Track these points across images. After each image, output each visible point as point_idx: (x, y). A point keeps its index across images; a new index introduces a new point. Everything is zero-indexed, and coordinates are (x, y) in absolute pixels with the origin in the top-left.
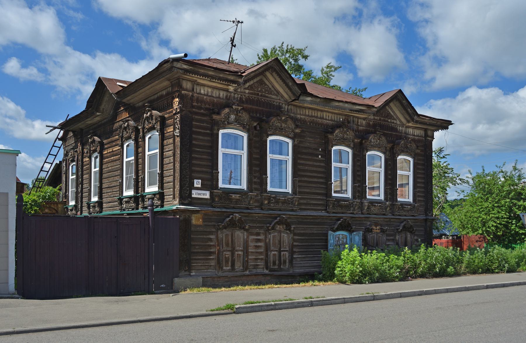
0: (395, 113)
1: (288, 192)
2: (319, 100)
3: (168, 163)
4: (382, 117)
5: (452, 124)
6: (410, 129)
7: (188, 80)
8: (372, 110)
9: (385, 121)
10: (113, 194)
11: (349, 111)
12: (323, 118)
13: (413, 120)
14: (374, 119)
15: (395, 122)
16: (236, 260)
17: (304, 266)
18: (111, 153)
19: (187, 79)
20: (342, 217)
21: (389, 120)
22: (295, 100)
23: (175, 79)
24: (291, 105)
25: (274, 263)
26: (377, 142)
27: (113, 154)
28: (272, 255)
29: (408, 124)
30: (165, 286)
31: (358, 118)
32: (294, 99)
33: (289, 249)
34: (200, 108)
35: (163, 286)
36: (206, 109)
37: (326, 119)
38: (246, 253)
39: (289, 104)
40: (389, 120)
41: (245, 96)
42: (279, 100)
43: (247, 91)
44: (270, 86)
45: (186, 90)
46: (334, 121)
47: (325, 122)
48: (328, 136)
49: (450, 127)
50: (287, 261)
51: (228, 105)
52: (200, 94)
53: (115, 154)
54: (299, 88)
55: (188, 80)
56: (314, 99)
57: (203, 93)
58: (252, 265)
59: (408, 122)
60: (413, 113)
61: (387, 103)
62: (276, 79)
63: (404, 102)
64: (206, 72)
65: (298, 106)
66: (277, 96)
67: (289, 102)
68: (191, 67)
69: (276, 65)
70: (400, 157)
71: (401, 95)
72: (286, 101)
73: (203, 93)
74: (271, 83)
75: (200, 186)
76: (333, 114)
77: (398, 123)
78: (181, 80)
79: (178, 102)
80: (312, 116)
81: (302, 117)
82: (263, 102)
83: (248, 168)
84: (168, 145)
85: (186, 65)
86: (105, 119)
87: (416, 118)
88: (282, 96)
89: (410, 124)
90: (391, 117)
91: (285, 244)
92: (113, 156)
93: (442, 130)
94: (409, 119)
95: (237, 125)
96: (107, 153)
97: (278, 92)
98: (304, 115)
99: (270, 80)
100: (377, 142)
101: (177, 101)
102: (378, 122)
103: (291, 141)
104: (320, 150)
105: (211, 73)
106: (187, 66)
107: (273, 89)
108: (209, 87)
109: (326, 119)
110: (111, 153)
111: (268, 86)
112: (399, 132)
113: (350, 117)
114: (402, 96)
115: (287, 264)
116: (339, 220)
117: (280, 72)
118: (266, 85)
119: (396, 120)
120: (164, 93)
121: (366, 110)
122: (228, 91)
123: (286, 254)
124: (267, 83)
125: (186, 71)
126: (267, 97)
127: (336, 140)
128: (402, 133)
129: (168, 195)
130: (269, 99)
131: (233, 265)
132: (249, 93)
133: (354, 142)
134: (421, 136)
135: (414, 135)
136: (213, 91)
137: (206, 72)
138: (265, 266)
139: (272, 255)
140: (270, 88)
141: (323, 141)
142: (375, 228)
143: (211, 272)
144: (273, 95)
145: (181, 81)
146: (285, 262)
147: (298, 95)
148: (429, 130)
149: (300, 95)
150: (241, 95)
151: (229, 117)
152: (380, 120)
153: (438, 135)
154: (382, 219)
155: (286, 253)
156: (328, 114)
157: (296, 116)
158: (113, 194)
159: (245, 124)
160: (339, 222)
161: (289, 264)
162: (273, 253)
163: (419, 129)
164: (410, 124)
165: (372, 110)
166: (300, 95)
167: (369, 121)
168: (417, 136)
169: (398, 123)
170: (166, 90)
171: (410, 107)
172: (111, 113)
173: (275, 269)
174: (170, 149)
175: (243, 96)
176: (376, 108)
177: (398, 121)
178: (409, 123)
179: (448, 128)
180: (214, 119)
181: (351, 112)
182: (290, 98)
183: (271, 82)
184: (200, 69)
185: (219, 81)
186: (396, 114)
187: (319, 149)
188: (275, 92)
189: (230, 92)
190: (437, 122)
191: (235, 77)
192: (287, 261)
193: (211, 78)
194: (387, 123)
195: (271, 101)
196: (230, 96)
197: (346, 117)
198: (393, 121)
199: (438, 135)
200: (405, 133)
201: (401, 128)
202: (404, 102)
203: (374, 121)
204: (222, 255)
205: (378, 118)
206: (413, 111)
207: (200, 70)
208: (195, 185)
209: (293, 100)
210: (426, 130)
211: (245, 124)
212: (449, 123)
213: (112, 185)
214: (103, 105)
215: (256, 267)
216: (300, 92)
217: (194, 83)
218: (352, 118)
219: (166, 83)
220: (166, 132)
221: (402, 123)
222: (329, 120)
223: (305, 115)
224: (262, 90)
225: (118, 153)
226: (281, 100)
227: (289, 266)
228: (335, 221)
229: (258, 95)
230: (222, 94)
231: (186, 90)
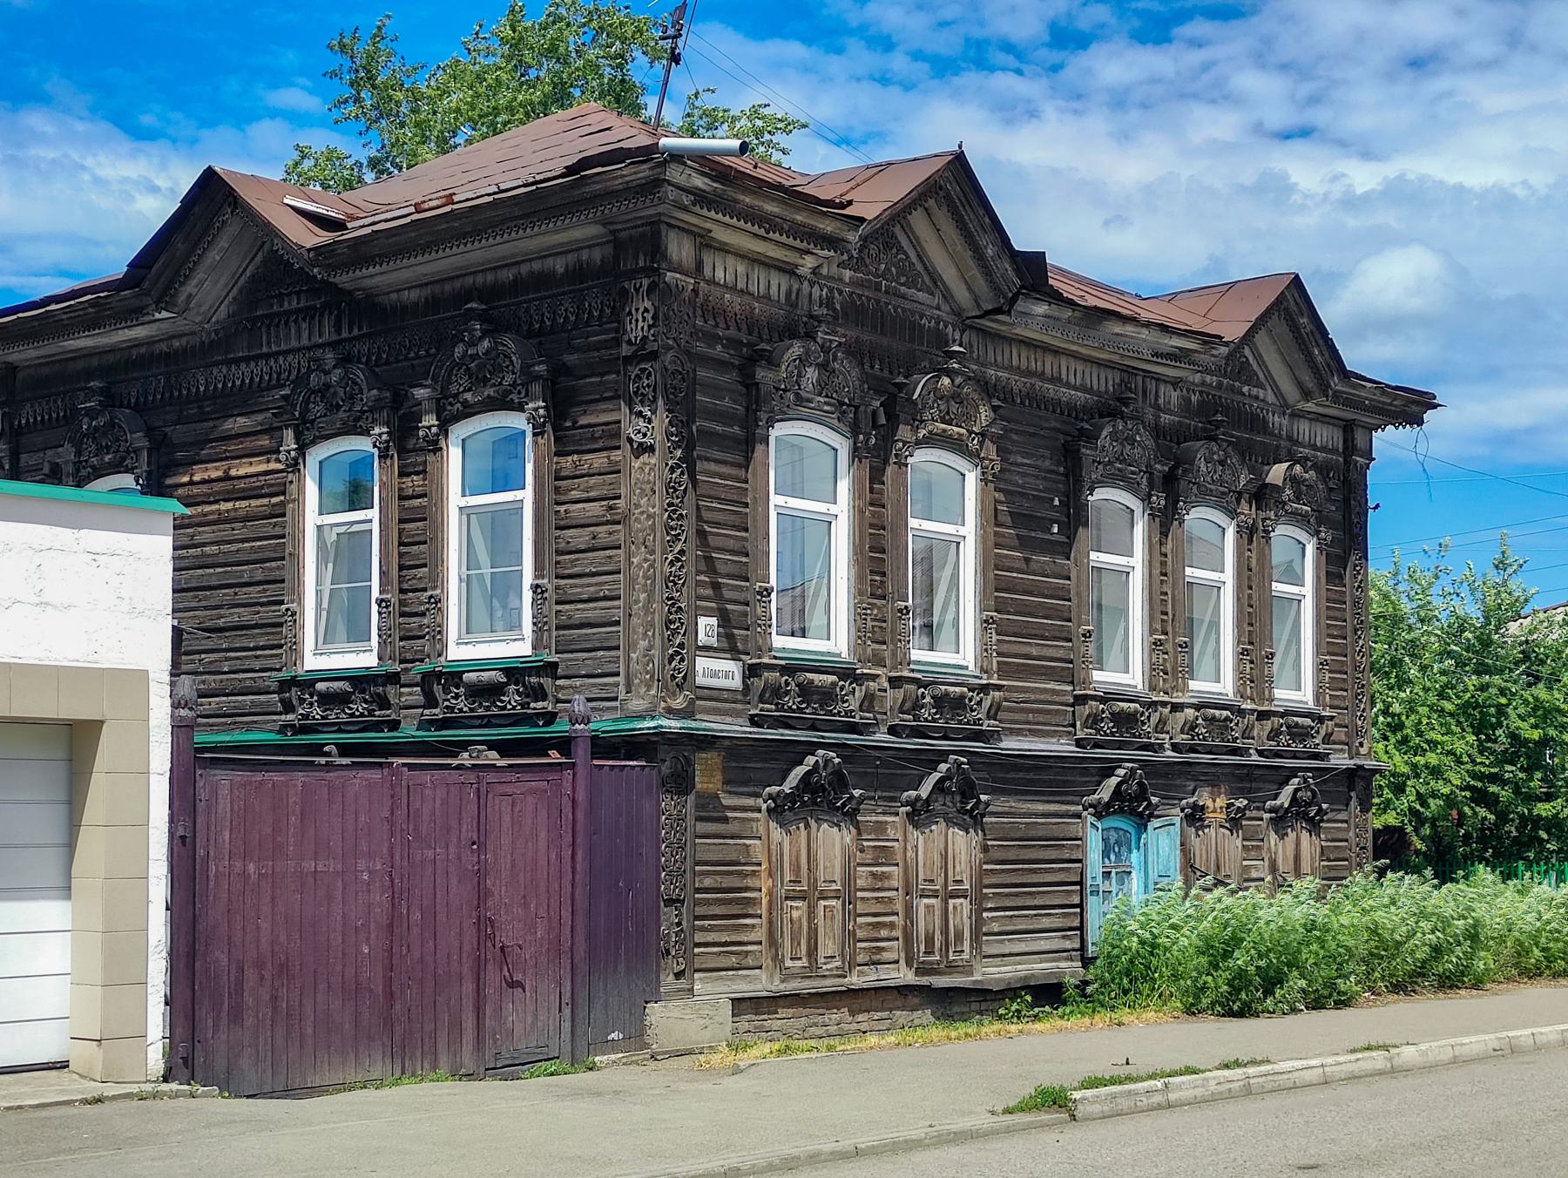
0: (1263, 362)
1: (963, 663)
2: (1067, 313)
3: (583, 547)
4: (1225, 376)
5: (1435, 406)
6: (1302, 420)
7: (683, 230)
8: (1214, 352)
9: (1232, 389)
10: (227, 659)
11: (1150, 358)
12: (1056, 380)
13: (1324, 388)
14: (1203, 383)
15: (1261, 396)
16: (821, 931)
17: (1011, 955)
18: (217, 487)
19: (681, 225)
20: (943, 755)
21: (1245, 389)
22: (998, 311)
23: (639, 222)
24: (971, 327)
25: (930, 940)
26: (1215, 472)
27: (228, 492)
28: (922, 910)
29: (1301, 405)
30: (621, 1036)
31: (1159, 379)
32: (990, 307)
33: (971, 886)
34: (712, 339)
35: (614, 1036)
36: (733, 343)
37: (1068, 385)
38: (850, 903)
39: (965, 324)
40: (1245, 389)
41: (840, 292)
42: (938, 308)
43: (847, 274)
44: (914, 259)
45: (678, 269)
46: (1090, 391)
47: (1066, 394)
48: (1079, 450)
49: (1429, 415)
50: (967, 934)
51: (790, 331)
52: (712, 282)
53: (244, 490)
54: (1018, 271)
55: (683, 230)
56: (1054, 310)
57: (722, 282)
58: (865, 949)
59: (1306, 395)
60: (1328, 365)
61: (899, 214)
62: (938, 230)
63: (1304, 320)
64: (757, 203)
65: (990, 334)
66: (932, 294)
67: (968, 318)
68: (715, 185)
69: (952, 178)
70: (1100, 494)
71: (1296, 295)
72: (957, 312)
73: (722, 282)
74: (916, 243)
75: (714, 642)
76: (1089, 364)
77: (1271, 398)
78: (663, 227)
79: (649, 316)
80: (1029, 373)
81: (1000, 374)
82: (891, 314)
83: (853, 572)
84: (582, 476)
85: (704, 174)
86: (180, 336)
87: (1335, 382)
88: (947, 296)
89: (1310, 406)
90: (1252, 380)
91: (958, 868)
92: (226, 500)
93: (1397, 428)
94: (1310, 383)
95: (826, 408)
96: (191, 483)
97: (936, 279)
98: (1006, 369)
99: (913, 233)
100: (1215, 472)
101: (646, 310)
102: (1214, 396)
103: (1139, 503)
104: (1056, 502)
105: (771, 208)
106: (707, 180)
107: (919, 267)
108: (740, 256)
109: (1068, 385)
110: (217, 487)
111: (905, 253)
112: (1272, 434)
113: (1136, 375)
114: (1299, 300)
115: (966, 946)
116: (1109, 773)
117: (962, 203)
118: (900, 249)
119: (1260, 385)
120: (559, 265)
121: (1196, 351)
122: (795, 273)
123: (961, 904)
124: (904, 243)
125: (701, 198)
126: (904, 297)
127: (1101, 467)
128: (1280, 436)
129: (583, 676)
130: (908, 305)
131: (812, 951)
132: (853, 283)
133: (1150, 473)
134: (1333, 451)
135: (1314, 447)
136: (750, 271)
137: (757, 203)
138: (903, 955)
139: (922, 910)
140: (913, 264)
141: (1062, 469)
142: (1209, 803)
143: (762, 983)
144: (919, 290)
145: (664, 234)
146: (959, 937)
147: (1010, 295)
148: (1360, 426)
149: (1016, 296)
150: (831, 290)
151: (800, 376)
152: (1220, 385)
153: (1388, 440)
154: (1228, 771)
155: (962, 900)
156: (1073, 364)
157: (983, 370)
158: (227, 659)
159: (846, 400)
160: (1114, 781)
161: (971, 945)
162: (926, 901)
163: (1328, 423)
164: (1310, 406)
165: (1214, 352)
166: (1016, 296)
167: (1188, 391)
168: (1324, 449)
169: (1271, 398)
170: (571, 258)
171: (1321, 342)
172: (222, 313)
173: (931, 963)
174: (592, 494)
175: (836, 294)
176: (1227, 344)
177: (1270, 391)
178: (1308, 401)
179: (1420, 423)
180: (758, 383)
181: (1155, 359)
182: (978, 305)
183: (917, 239)
184: (743, 193)
185: (713, 212)
186: (1266, 367)
187: (1053, 500)
188: (927, 279)
189: (799, 277)
190: (1395, 400)
191: (839, 224)
192: (967, 934)
193: (769, 223)
194: (1240, 398)
195: (913, 313)
196: (798, 291)
197: (1125, 375)
198: (1255, 391)
199: (1388, 440)
200: (1290, 438)
201: (1276, 419)
202: (1304, 320)
203: (1201, 393)
204: (782, 909)
205: (1215, 378)
206: (1327, 355)
207: (741, 197)
208: (702, 638)
209: (986, 314)
210: (1348, 428)
211: (844, 404)
212: (1426, 402)
213: (221, 622)
214: (194, 282)
215: (875, 958)
216: (1018, 282)
217: (705, 242)
218: (1140, 379)
219: (593, 230)
220: (568, 424)
221: (1283, 397)
222: (1075, 388)
223: (1010, 368)
224: (889, 270)
225: (262, 487)
226: (943, 308)
227: (971, 952)
228: (1097, 778)
229: (878, 288)
230: (778, 284)
231: (678, 269)
